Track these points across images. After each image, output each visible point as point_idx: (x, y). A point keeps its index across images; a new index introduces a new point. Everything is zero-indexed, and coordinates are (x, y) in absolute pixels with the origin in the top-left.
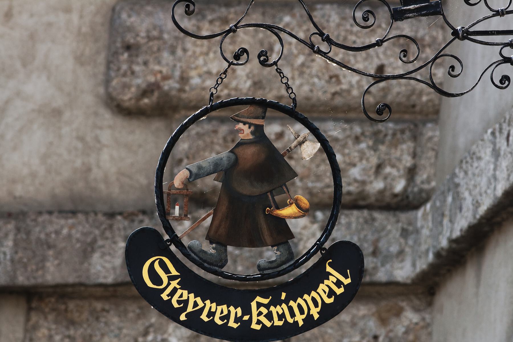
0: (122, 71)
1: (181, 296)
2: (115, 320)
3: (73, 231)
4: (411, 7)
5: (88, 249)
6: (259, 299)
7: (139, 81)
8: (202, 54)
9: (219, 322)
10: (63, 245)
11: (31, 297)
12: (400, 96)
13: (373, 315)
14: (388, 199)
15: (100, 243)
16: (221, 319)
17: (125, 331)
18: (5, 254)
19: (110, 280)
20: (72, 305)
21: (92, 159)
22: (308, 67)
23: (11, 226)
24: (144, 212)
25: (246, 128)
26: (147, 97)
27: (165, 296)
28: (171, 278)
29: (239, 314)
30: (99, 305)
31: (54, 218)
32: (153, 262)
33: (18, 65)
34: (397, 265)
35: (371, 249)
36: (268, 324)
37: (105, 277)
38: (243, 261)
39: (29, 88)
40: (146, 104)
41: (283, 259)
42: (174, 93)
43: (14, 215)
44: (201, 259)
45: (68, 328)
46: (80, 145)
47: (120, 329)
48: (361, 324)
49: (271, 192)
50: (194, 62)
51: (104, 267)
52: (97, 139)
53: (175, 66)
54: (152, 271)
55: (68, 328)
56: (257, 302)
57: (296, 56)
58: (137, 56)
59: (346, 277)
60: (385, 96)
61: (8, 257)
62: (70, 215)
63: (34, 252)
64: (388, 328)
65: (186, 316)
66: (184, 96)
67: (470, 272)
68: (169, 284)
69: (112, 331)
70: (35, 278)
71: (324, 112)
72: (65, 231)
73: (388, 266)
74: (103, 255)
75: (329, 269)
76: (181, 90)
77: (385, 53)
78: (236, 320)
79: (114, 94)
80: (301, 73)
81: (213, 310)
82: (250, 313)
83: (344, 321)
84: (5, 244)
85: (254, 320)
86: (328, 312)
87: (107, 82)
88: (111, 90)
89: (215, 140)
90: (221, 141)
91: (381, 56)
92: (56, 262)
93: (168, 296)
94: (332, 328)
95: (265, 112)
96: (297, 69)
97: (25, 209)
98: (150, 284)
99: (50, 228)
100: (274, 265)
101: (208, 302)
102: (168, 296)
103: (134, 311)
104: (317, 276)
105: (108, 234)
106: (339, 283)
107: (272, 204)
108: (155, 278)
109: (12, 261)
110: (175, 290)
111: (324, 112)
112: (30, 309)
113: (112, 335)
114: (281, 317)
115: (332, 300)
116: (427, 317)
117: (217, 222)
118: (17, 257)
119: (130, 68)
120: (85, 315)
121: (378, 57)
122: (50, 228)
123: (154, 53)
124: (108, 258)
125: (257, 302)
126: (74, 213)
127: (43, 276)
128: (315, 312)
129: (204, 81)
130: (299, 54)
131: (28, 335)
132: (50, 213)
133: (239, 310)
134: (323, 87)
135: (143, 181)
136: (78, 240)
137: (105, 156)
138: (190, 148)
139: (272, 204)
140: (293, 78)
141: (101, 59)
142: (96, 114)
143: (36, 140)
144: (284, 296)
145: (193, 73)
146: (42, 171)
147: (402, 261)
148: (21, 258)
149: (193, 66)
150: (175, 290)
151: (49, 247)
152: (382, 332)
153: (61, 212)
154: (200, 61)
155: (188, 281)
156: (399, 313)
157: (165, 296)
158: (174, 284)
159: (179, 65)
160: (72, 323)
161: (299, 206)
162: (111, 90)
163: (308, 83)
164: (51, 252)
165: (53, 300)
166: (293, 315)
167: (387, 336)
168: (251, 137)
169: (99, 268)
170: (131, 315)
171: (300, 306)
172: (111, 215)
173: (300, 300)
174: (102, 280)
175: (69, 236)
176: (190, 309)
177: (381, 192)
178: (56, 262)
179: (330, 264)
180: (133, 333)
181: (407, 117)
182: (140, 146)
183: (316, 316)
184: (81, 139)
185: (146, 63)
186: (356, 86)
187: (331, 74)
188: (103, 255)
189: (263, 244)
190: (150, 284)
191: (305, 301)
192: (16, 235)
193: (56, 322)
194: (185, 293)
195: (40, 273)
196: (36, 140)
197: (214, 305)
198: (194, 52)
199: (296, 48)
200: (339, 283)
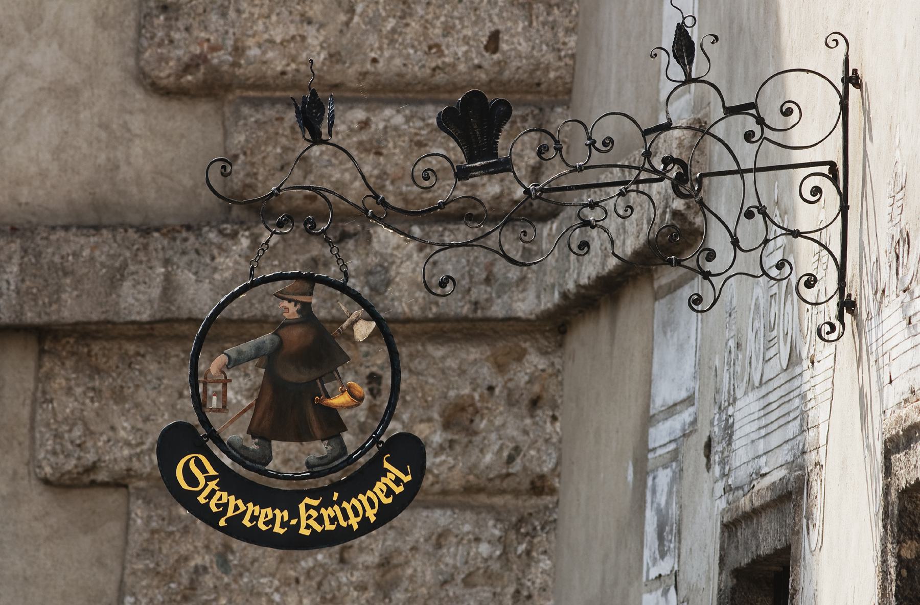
0: (157, 40)
1: (220, 499)
2: (153, 367)
3: (97, 253)
4: (477, 164)
5: (116, 277)
6: (307, 500)
7: (180, 52)
8: (261, 16)
9: (263, 528)
10: (85, 270)
11: (44, 337)
12: (521, 71)
13: (487, 359)
14: (505, 206)
15: (132, 268)
16: (266, 523)
17: (165, 381)
18: (8, 282)
19: (145, 317)
20: (96, 348)
21: (120, 154)
22: (400, 34)
23: (15, 246)
24: (189, 228)
25: (291, 306)
26: (191, 74)
27: (201, 499)
28: (209, 479)
29: (286, 518)
30: (131, 348)
31: (71, 235)
32: (189, 460)
33: (21, 29)
34: (517, 295)
35: (484, 276)
36: (319, 529)
37: (139, 313)
38: (288, 457)
39: (35, 60)
40: (189, 82)
41: (335, 454)
42: (225, 68)
43: (17, 229)
44: (242, 456)
45: (92, 378)
46: (103, 135)
47: (159, 379)
48: (472, 371)
49: (320, 378)
50: (251, 27)
51: (137, 300)
52: (126, 127)
53: (227, 32)
54: (187, 470)
55: (92, 378)
56: (306, 504)
57: (385, 20)
58: (177, 19)
59: (406, 474)
60: (500, 72)
61: (12, 287)
62: (92, 231)
63: (46, 280)
64: (506, 378)
65: (226, 521)
66: (239, 72)
67: (604, 321)
68: (206, 485)
69: (149, 382)
70: (47, 314)
71: (422, 92)
72: (86, 253)
73: (505, 297)
74: (136, 283)
75: (386, 465)
76: (235, 64)
77: (500, 15)
78: (283, 525)
79: (147, 69)
80: (392, 42)
81: (256, 514)
82: (297, 516)
83: (450, 368)
84: (8, 270)
85: (303, 524)
86: (386, 514)
87: (138, 52)
88: (142, 63)
89: (281, 131)
90: (288, 132)
91: (496, 19)
92: (75, 293)
93: (205, 498)
94: (434, 377)
95: (312, 288)
96: (387, 38)
97: (34, 220)
98: (184, 486)
99: (66, 249)
100: (325, 461)
101: (250, 505)
102: (205, 498)
103: (177, 356)
104: (374, 472)
105: (142, 256)
106: (398, 481)
107: (322, 392)
108: (191, 479)
109: (18, 292)
110: (213, 492)
111: (422, 92)
112: (42, 352)
113: (148, 386)
114: (333, 520)
115: (390, 500)
116: (557, 361)
117: (259, 414)
118: (24, 287)
119: (168, 35)
120: (115, 360)
121: (491, 21)
122: (66, 249)
123: (200, 15)
124: (142, 287)
125: (306, 504)
126: (97, 228)
127: (59, 311)
128: (371, 514)
129: (264, 53)
130: (389, 16)
131: (40, 386)
132: (66, 228)
133: (286, 513)
134: (420, 61)
135: (188, 182)
136: (103, 265)
137: (137, 150)
138: (247, 141)
139: (322, 392)
140: (381, 48)
141: (130, 20)
142: (124, 93)
143: (47, 127)
144: (336, 496)
145: (250, 42)
146: (54, 169)
147: (524, 290)
148: (29, 288)
149: (250, 32)
150: (213, 492)
151: (66, 274)
152: (499, 383)
153: (79, 227)
154: (260, 26)
155: (228, 481)
156: (520, 357)
157: (201, 499)
158: (212, 485)
159: (231, 31)
160: (97, 371)
161: (352, 394)
162: (142, 63)
163: (400, 55)
164: (68, 281)
165: (72, 341)
166: (346, 518)
167: (505, 387)
168: (297, 316)
169: (131, 300)
170: (173, 360)
171: (354, 508)
172: (145, 231)
173: (354, 501)
174: (135, 317)
175: (92, 259)
176: (230, 513)
177: (498, 198)
178: (75, 293)
179: (387, 460)
180: (177, 384)
181: (530, 97)
182: (182, 136)
183: (373, 519)
184: (104, 126)
185: (187, 29)
186: (463, 59)
187: (431, 42)
188: (136, 283)
189: (312, 438)
190: (184, 486)
191: (360, 501)
192: (22, 258)
193: (76, 370)
194: (225, 494)
195: (54, 307)
196: (47, 127)
197: (257, 508)
198: (252, 14)
199: (385, 9)
200: (398, 481)
